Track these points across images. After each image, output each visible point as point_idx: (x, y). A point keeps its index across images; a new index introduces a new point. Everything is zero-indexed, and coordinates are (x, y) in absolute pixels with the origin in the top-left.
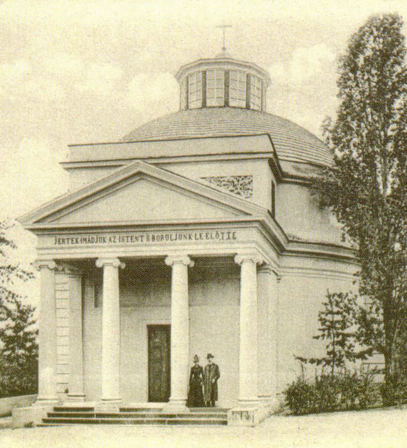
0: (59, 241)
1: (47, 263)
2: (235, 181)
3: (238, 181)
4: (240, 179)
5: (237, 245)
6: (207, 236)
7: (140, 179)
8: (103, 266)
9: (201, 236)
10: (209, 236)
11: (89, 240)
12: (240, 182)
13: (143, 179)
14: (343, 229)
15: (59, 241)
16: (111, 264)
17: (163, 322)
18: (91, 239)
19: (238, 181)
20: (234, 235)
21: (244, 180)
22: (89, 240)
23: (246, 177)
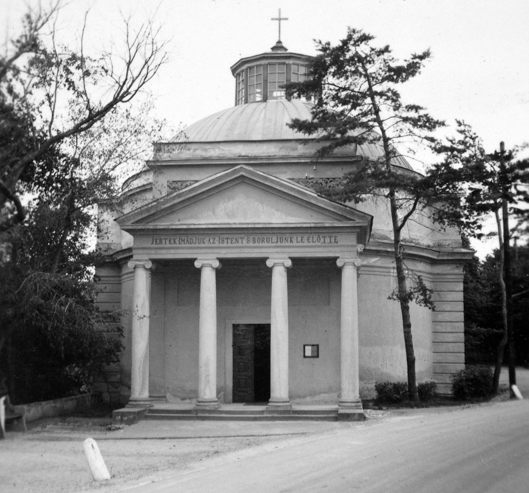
0: (156, 242)
1: (210, 262)
2: (323, 182)
3: (327, 183)
4: (328, 182)
5: (337, 249)
6: (308, 240)
7: (241, 182)
8: (273, 266)
9: (302, 240)
10: (311, 240)
11: (188, 241)
12: (328, 185)
13: (244, 182)
14: (108, 214)
15: (156, 242)
16: (211, 266)
17: (269, 323)
18: (189, 240)
19: (327, 183)
20: (335, 240)
21: (333, 183)
22: (188, 241)
23: (334, 179)
